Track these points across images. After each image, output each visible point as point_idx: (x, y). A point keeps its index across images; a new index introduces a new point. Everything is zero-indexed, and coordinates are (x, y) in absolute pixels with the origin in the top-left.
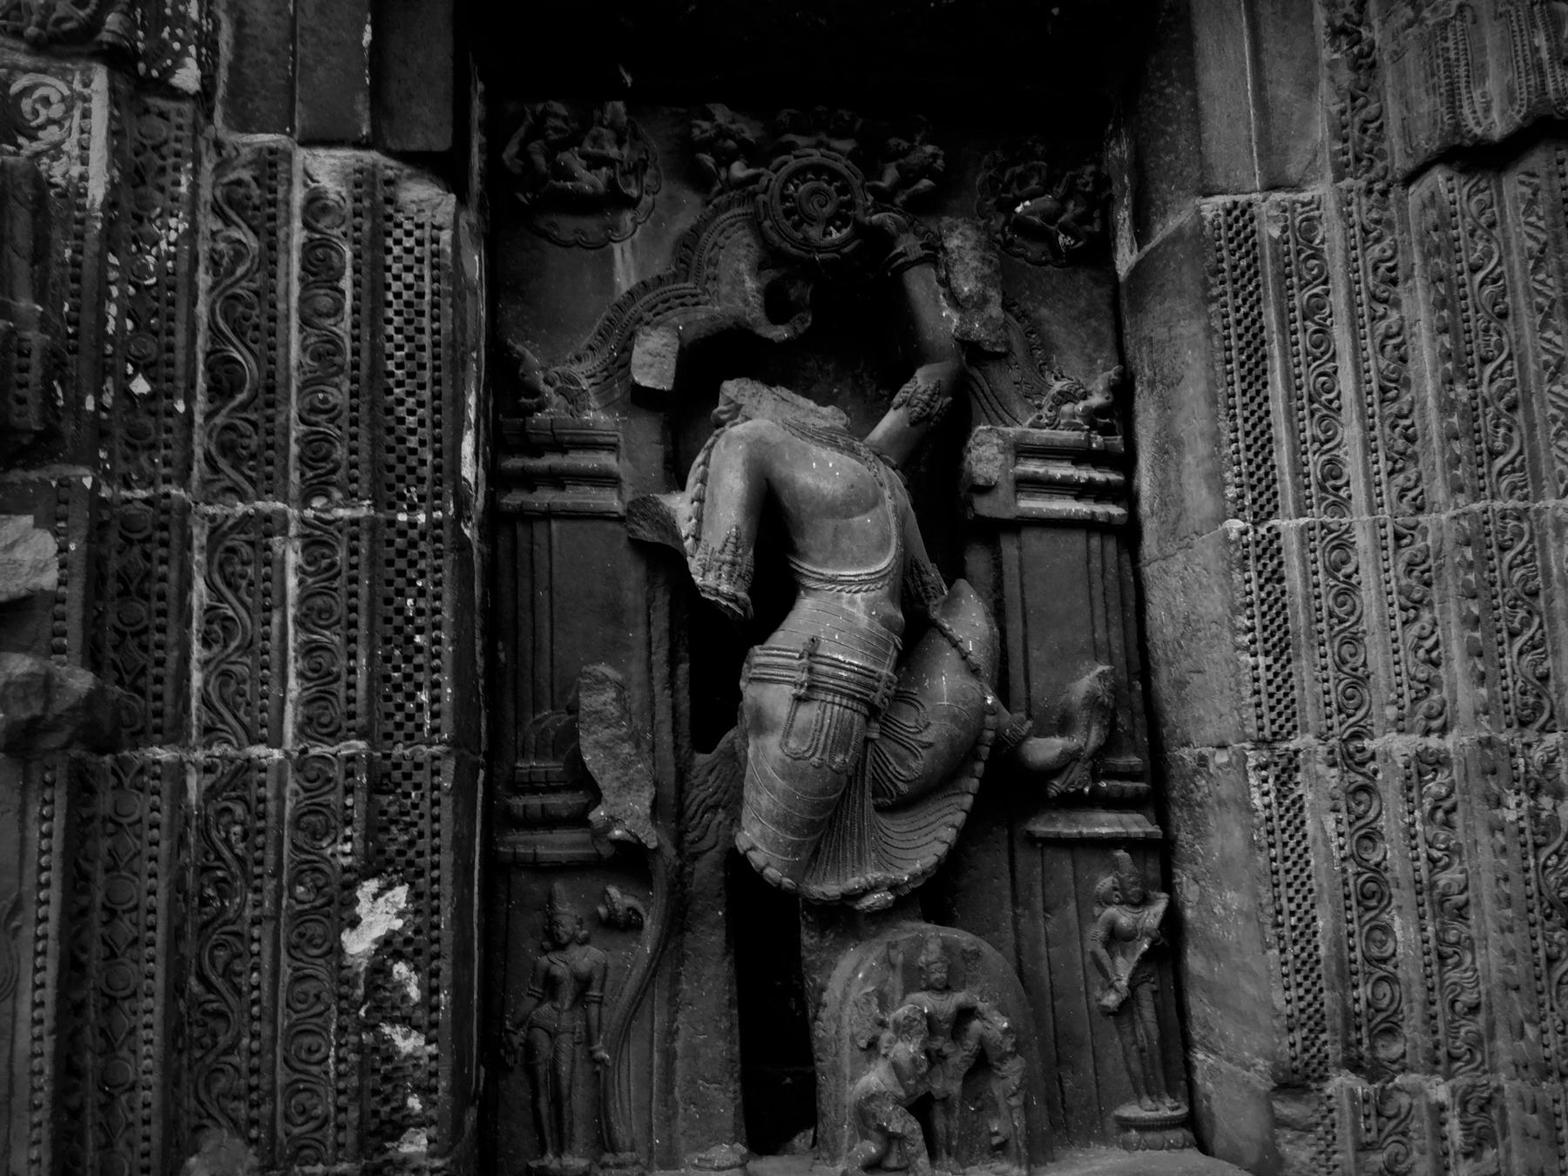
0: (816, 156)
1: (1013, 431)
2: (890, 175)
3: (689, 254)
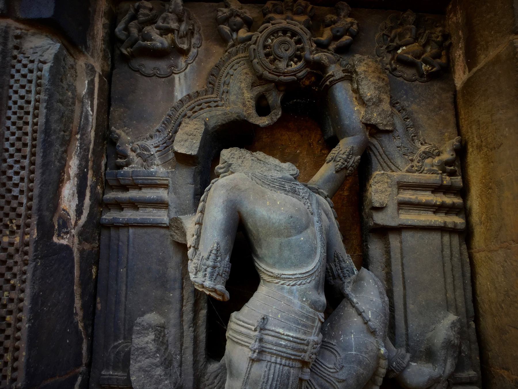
0: (284, 24)
1: (396, 175)
2: (326, 35)
3: (213, 80)
